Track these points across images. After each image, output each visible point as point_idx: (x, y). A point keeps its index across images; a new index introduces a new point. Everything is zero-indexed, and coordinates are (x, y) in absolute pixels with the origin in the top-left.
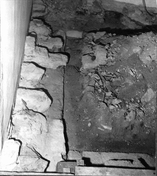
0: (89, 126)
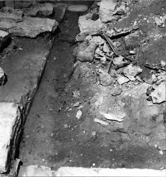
0: (79, 118)
